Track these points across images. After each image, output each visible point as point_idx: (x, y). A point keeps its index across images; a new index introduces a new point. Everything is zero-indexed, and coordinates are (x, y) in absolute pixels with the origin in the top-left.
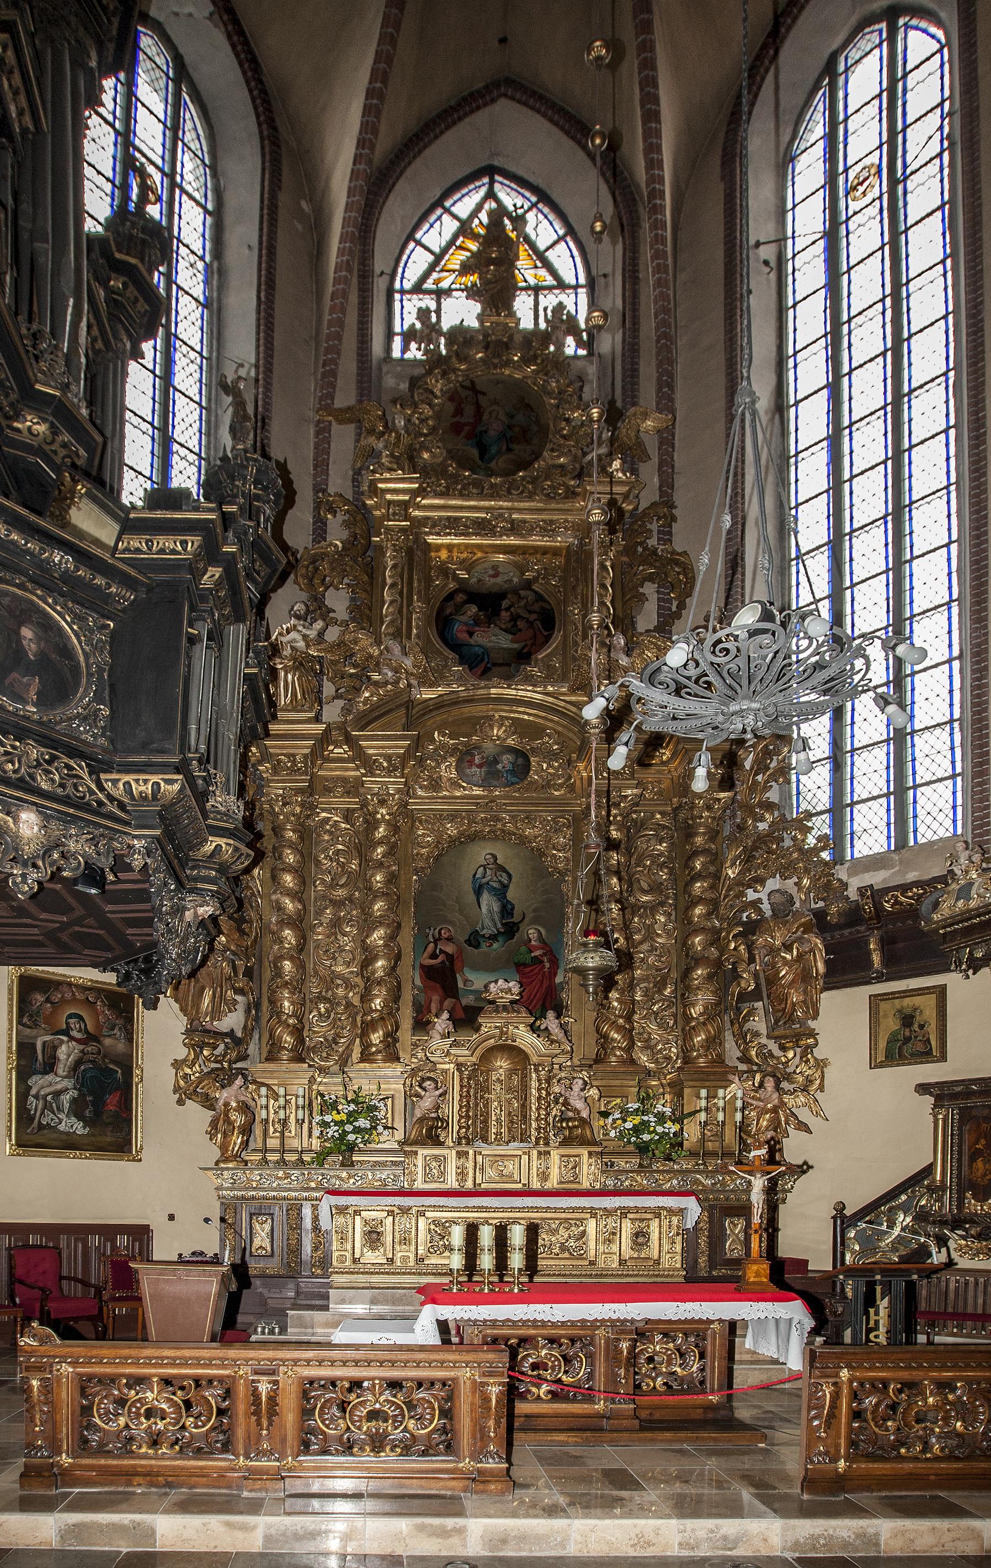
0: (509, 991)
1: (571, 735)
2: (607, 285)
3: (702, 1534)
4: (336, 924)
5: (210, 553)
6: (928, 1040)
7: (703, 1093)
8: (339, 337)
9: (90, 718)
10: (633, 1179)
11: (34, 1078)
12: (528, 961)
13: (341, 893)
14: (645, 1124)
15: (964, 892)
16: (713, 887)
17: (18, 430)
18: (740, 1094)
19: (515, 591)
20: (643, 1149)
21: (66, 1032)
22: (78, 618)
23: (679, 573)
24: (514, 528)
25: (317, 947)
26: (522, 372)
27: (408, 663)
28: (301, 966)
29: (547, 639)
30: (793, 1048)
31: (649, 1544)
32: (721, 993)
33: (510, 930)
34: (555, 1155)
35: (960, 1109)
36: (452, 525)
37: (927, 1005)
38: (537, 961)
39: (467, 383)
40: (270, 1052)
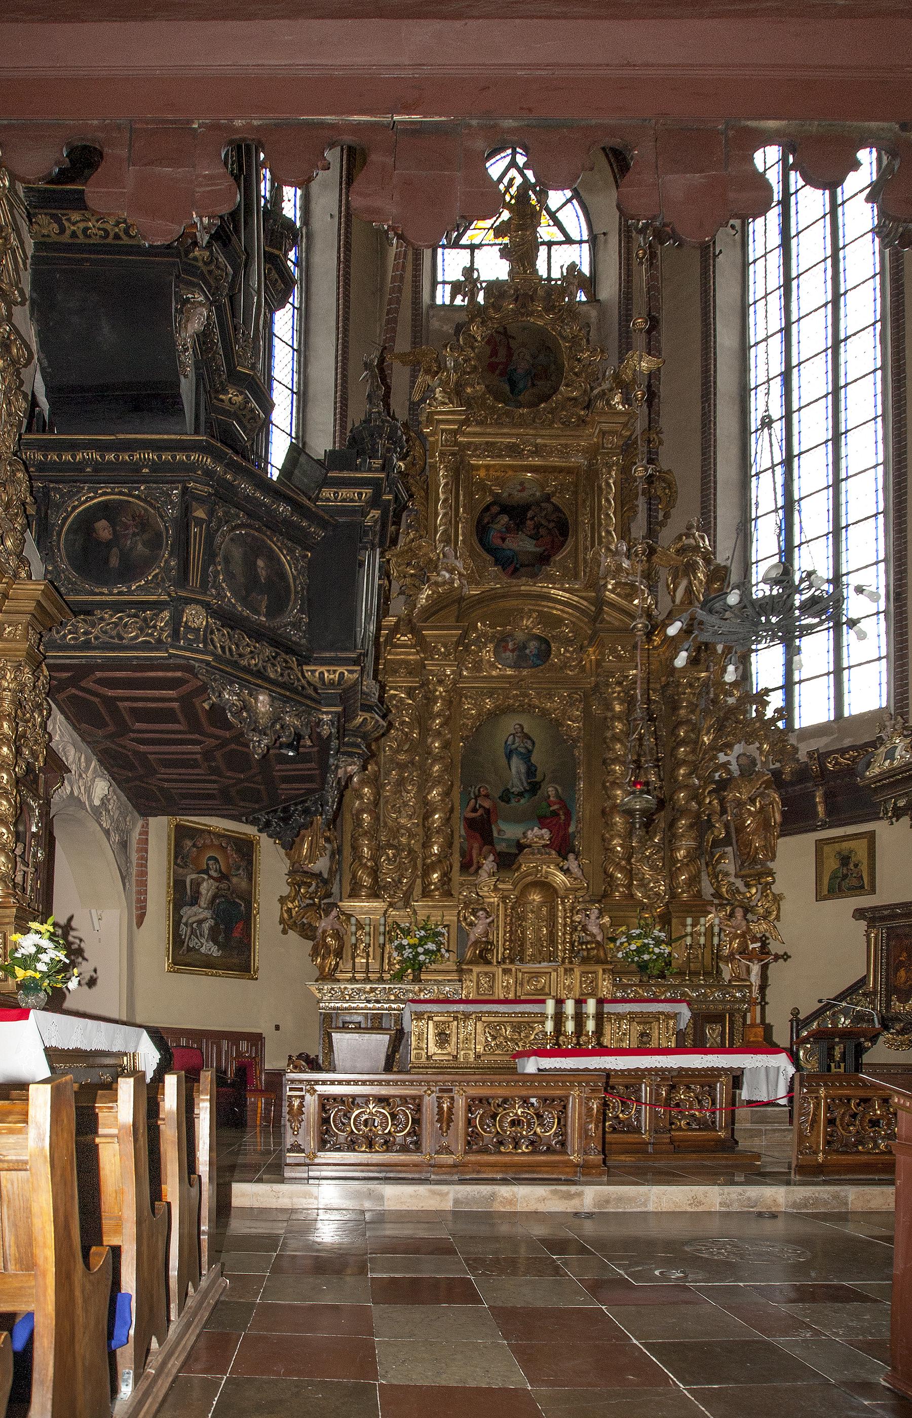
0: (541, 837)
1: (582, 625)
2: (606, 241)
3: (734, 1196)
4: (401, 783)
5: (375, 501)
6: (861, 877)
7: (689, 921)
8: (400, 290)
9: (296, 625)
10: (636, 992)
11: (185, 909)
12: (548, 814)
13: (402, 757)
14: (646, 945)
15: (890, 755)
16: (693, 751)
17: (222, 401)
18: (717, 921)
19: (538, 503)
20: (643, 967)
21: (206, 872)
22: (291, 551)
23: (665, 488)
24: (538, 451)
25: (387, 802)
26: (542, 321)
27: (459, 564)
28: (376, 818)
29: (563, 544)
30: (755, 885)
31: (700, 1203)
32: (700, 838)
33: (534, 788)
34: (577, 972)
35: (888, 928)
36: (490, 449)
37: (860, 847)
38: (555, 814)
39: (501, 330)
40: (352, 890)
